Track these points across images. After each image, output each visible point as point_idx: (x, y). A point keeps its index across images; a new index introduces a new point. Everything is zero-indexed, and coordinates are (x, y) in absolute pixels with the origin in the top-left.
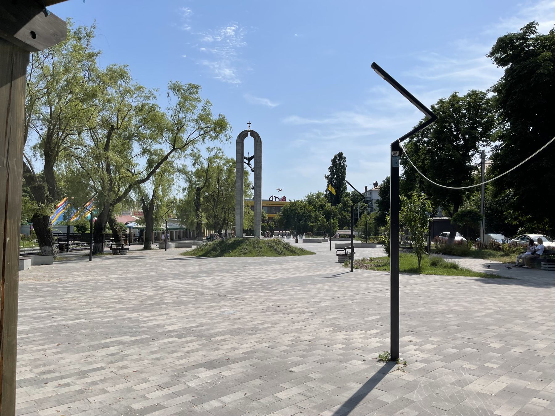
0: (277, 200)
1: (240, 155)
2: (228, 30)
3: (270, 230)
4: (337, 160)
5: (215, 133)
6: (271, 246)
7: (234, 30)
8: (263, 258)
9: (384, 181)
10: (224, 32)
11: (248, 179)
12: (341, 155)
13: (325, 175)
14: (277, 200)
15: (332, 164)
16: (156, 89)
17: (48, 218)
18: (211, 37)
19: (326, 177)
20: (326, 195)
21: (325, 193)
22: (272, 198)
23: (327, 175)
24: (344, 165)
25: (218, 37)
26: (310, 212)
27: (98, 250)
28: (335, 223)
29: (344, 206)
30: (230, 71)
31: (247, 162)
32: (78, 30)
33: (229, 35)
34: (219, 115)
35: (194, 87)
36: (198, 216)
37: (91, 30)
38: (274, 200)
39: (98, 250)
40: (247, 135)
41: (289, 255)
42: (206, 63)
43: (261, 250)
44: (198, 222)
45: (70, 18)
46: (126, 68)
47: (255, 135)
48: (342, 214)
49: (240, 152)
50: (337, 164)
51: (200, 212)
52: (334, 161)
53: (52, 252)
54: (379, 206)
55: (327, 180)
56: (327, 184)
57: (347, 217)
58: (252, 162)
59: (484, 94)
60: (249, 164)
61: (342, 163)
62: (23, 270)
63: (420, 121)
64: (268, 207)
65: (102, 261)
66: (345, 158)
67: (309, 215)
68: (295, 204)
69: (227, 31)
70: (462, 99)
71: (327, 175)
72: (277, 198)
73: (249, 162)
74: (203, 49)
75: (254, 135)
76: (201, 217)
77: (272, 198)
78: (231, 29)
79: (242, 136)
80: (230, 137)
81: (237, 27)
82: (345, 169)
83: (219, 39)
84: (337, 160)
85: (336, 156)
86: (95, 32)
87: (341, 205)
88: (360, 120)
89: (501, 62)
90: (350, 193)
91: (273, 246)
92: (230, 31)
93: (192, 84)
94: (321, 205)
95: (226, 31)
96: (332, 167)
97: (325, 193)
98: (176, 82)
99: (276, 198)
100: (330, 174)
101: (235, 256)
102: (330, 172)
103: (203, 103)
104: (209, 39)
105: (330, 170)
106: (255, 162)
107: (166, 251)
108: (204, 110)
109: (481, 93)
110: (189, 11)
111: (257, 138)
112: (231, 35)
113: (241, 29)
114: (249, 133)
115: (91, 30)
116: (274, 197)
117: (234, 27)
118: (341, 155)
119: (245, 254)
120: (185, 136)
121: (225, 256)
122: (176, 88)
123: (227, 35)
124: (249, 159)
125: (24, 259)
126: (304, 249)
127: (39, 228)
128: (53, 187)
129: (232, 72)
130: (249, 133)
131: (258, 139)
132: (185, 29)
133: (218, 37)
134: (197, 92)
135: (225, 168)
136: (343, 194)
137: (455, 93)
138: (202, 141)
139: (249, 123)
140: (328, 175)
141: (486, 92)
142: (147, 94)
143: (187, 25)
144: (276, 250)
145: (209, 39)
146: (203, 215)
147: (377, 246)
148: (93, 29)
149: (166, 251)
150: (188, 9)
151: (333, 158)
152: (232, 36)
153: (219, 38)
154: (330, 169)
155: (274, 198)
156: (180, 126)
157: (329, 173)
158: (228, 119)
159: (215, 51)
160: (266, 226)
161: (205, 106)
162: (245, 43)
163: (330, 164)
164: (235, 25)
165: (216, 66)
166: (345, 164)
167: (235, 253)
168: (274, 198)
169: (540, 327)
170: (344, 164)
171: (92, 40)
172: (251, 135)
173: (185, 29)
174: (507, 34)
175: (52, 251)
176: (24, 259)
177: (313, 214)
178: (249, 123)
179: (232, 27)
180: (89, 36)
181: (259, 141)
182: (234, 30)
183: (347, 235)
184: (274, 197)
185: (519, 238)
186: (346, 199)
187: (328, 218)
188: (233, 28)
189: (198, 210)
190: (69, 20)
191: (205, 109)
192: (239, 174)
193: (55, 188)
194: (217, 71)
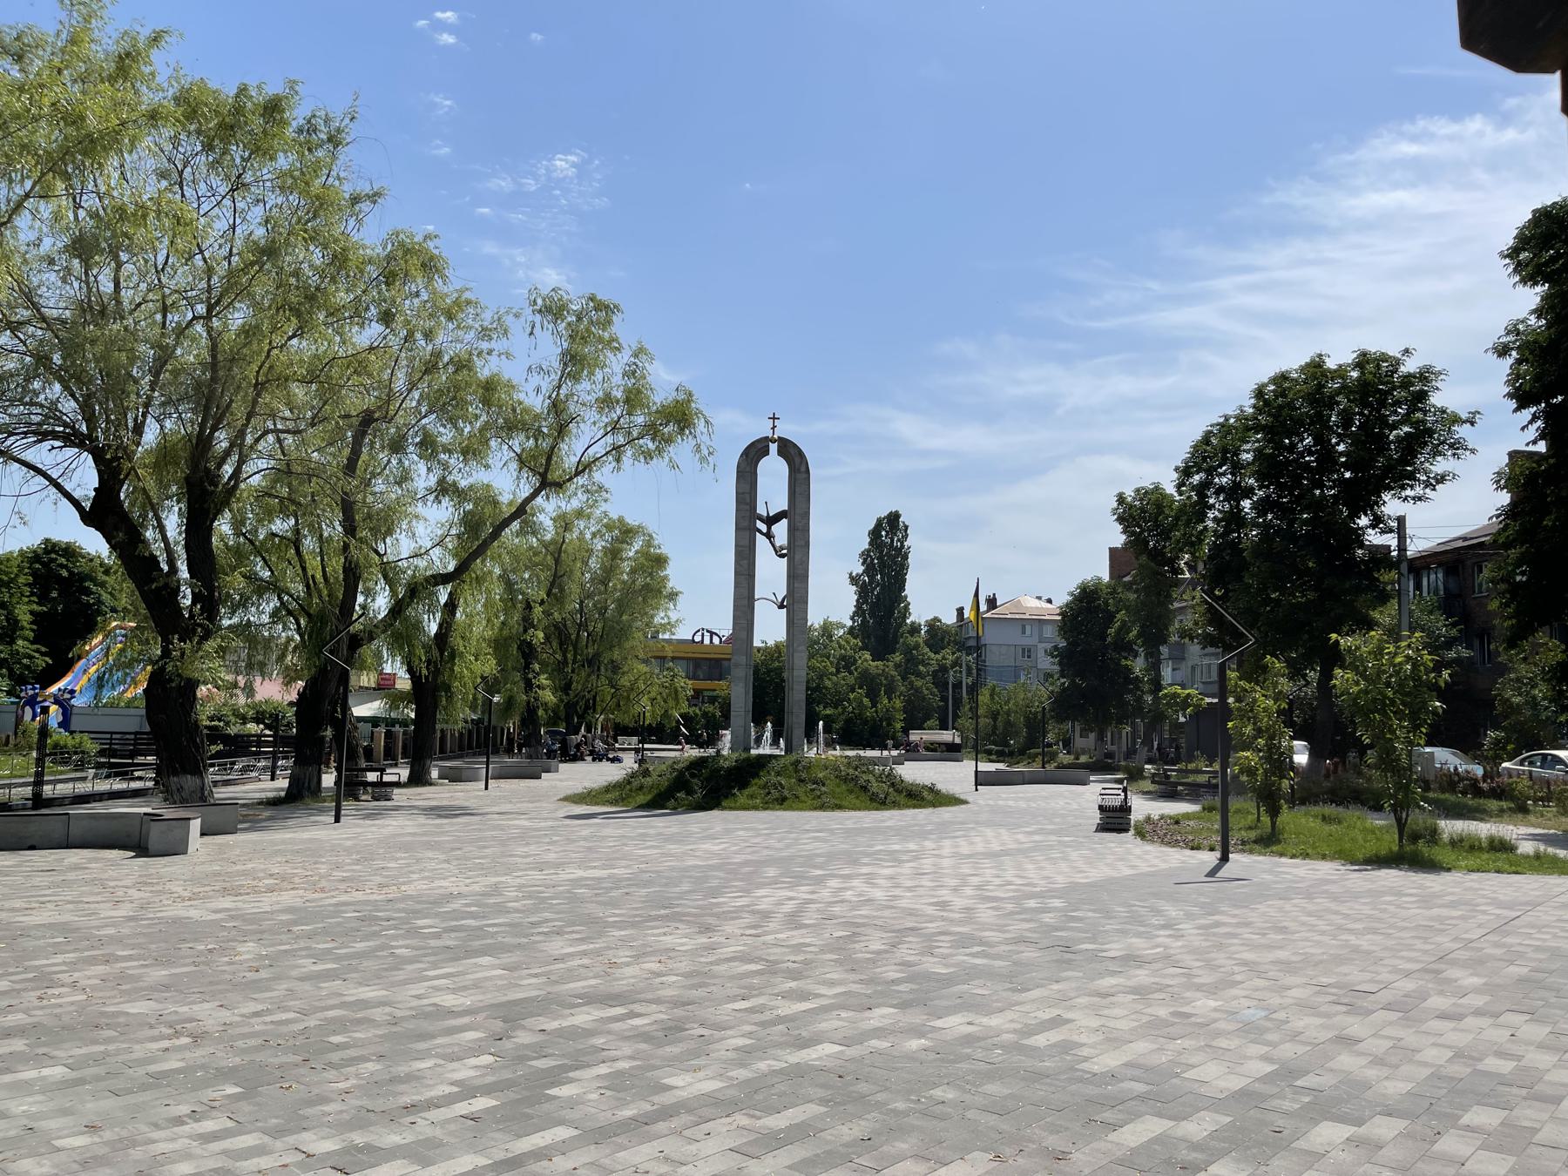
0: (716, 640)
1: (748, 507)
2: (558, 163)
3: (706, 727)
4: (883, 533)
5: (653, 440)
6: (846, 779)
7: (574, 165)
8: (838, 814)
9: (1071, 594)
10: (547, 169)
11: (666, 578)
12: (893, 518)
13: (851, 574)
14: (716, 640)
15: (870, 544)
16: (514, 311)
17: (193, 685)
18: (509, 179)
19: (854, 580)
20: (852, 628)
21: (849, 623)
22: (700, 633)
23: (854, 574)
24: (902, 546)
25: (529, 181)
26: (821, 677)
27: (306, 784)
28: (893, 708)
29: (908, 661)
30: (558, 274)
31: (763, 527)
32: (309, 122)
33: (561, 176)
34: (677, 389)
35: (601, 306)
36: (529, 685)
37: (343, 124)
38: (707, 641)
39: (306, 784)
40: (765, 452)
41: (908, 807)
42: (490, 248)
43: (823, 789)
44: (528, 703)
45: (294, 82)
46: (431, 244)
47: (792, 451)
48: (911, 683)
49: (748, 501)
50: (883, 544)
51: (533, 671)
52: (875, 534)
53: (203, 794)
54: (1060, 664)
55: (854, 588)
56: (856, 597)
57: (926, 692)
58: (781, 530)
59: (1396, 363)
60: (769, 536)
61: (898, 540)
62: (185, 852)
63: (1206, 429)
64: (688, 659)
65: (361, 822)
66: (906, 527)
67: (818, 686)
68: (780, 653)
69: (555, 165)
70: (1341, 372)
71: (854, 574)
72: (716, 634)
73: (769, 528)
74: (486, 210)
75: (789, 451)
76: (538, 687)
77: (700, 633)
78: (567, 161)
79: (754, 453)
80: (710, 453)
81: (586, 155)
82: (906, 557)
83: (531, 185)
84: (883, 533)
85: (879, 523)
86: (353, 132)
87: (898, 657)
88: (908, 427)
89: (1529, 273)
90: (920, 625)
91: (852, 779)
92: (563, 164)
93: (599, 298)
94: (843, 658)
95: (553, 165)
96: (868, 551)
97: (849, 623)
98: (553, 290)
99: (712, 634)
100: (864, 572)
101: (755, 808)
102: (863, 564)
103: (625, 357)
104: (504, 184)
105: (865, 560)
106: (792, 530)
107: (486, 788)
108: (630, 373)
109: (1384, 357)
110: (448, 103)
111: (797, 460)
112: (565, 178)
113: (597, 162)
114: (773, 447)
115: (343, 124)
116: (708, 631)
117: (576, 154)
118: (893, 518)
119: (781, 802)
120: (571, 452)
121: (724, 808)
122: (553, 310)
123: (555, 175)
124: (771, 521)
125: (189, 819)
126: (939, 786)
127: (164, 716)
128: (211, 589)
129: (564, 278)
130: (773, 447)
131: (801, 463)
132: (435, 152)
133: (529, 181)
134: (609, 322)
135: (599, 545)
136: (900, 625)
137: (1320, 356)
138: (614, 464)
139: (774, 418)
140: (857, 575)
141: (1399, 356)
142: (485, 324)
143: (439, 142)
144: (864, 789)
145: (503, 184)
146: (544, 681)
147: (1092, 778)
148: (347, 121)
149: (486, 788)
150: (447, 99)
151: (872, 526)
152: (567, 180)
153: (532, 182)
154: (865, 555)
155: (706, 633)
156: (561, 419)
157: (860, 569)
158: (700, 403)
159: (517, 217)
160: (696, 715)
161: (635, 363)
162: (605, 199)
163: (864, 543)
164: (578, 151)
165: (518, 259)
166: (905, 543)
167: (752, 797)
168: (706, 633)
169: (1481, 1003)
170: (902, 543)
171: (344, 154)
172: (780, 453)
173: (435, 152)
174: (1558, 199)
175: (202, 789)
176: (189, 819)
177: (828, 683)
178: (774, 418)
179: (571, 154)
180: (334, 140)
181: (803, 469)
182: (574, 165)
183: (940, 744)
184: (708, 631)
185: (1524, 759)
186: (912, 640)
187: (873, 695)
188: (572, 158)
189: (527, 666)
190: (292, 88)
191: (634, 372)
192: (742, 563)
193: (216, 594)
194: (521, 272)
